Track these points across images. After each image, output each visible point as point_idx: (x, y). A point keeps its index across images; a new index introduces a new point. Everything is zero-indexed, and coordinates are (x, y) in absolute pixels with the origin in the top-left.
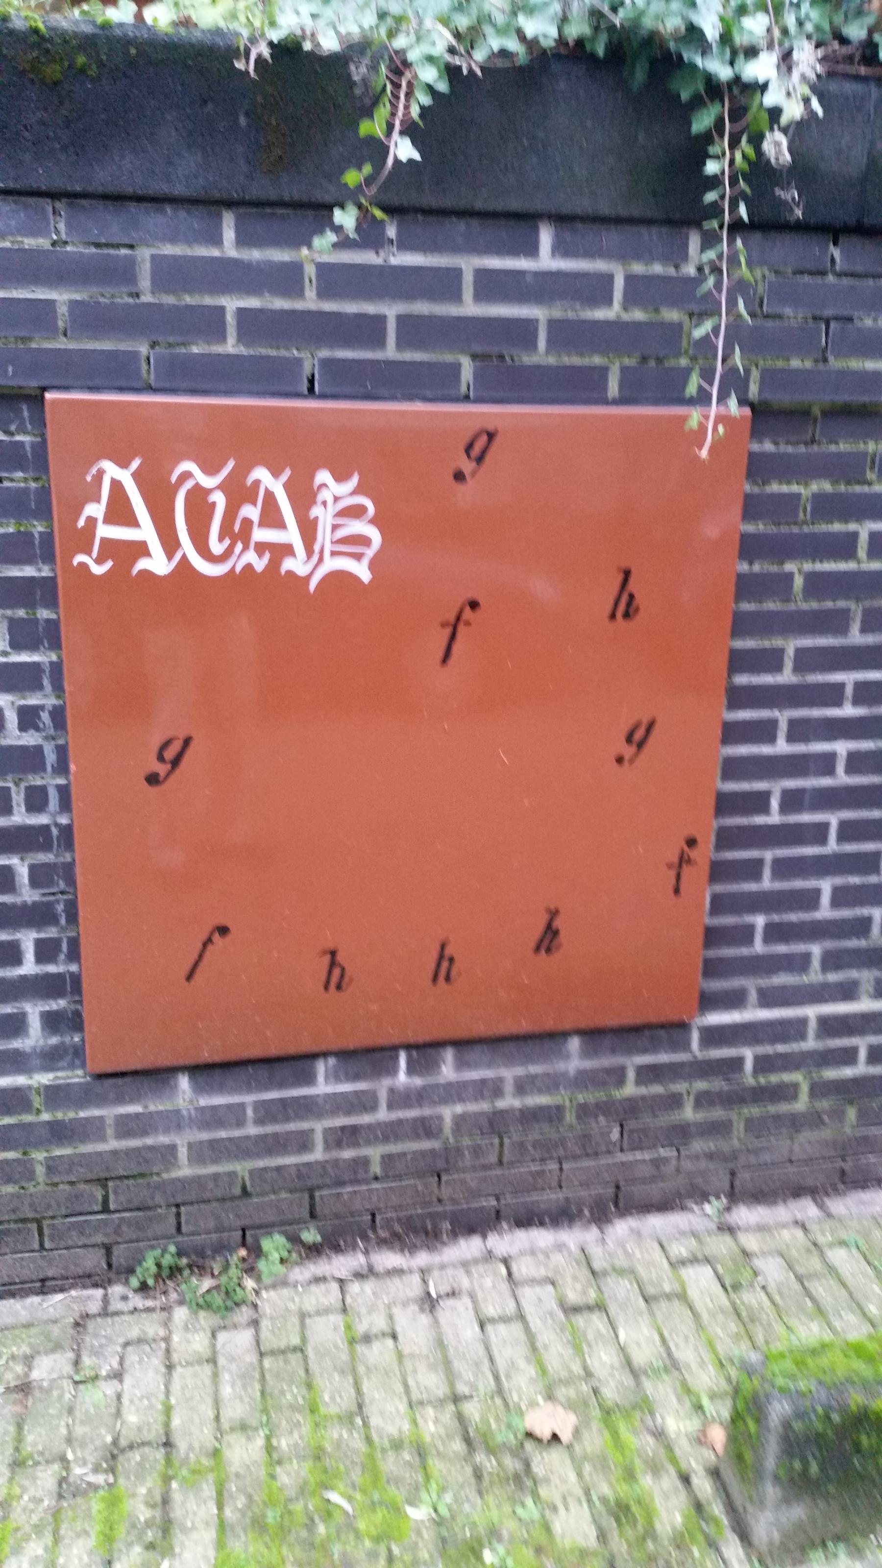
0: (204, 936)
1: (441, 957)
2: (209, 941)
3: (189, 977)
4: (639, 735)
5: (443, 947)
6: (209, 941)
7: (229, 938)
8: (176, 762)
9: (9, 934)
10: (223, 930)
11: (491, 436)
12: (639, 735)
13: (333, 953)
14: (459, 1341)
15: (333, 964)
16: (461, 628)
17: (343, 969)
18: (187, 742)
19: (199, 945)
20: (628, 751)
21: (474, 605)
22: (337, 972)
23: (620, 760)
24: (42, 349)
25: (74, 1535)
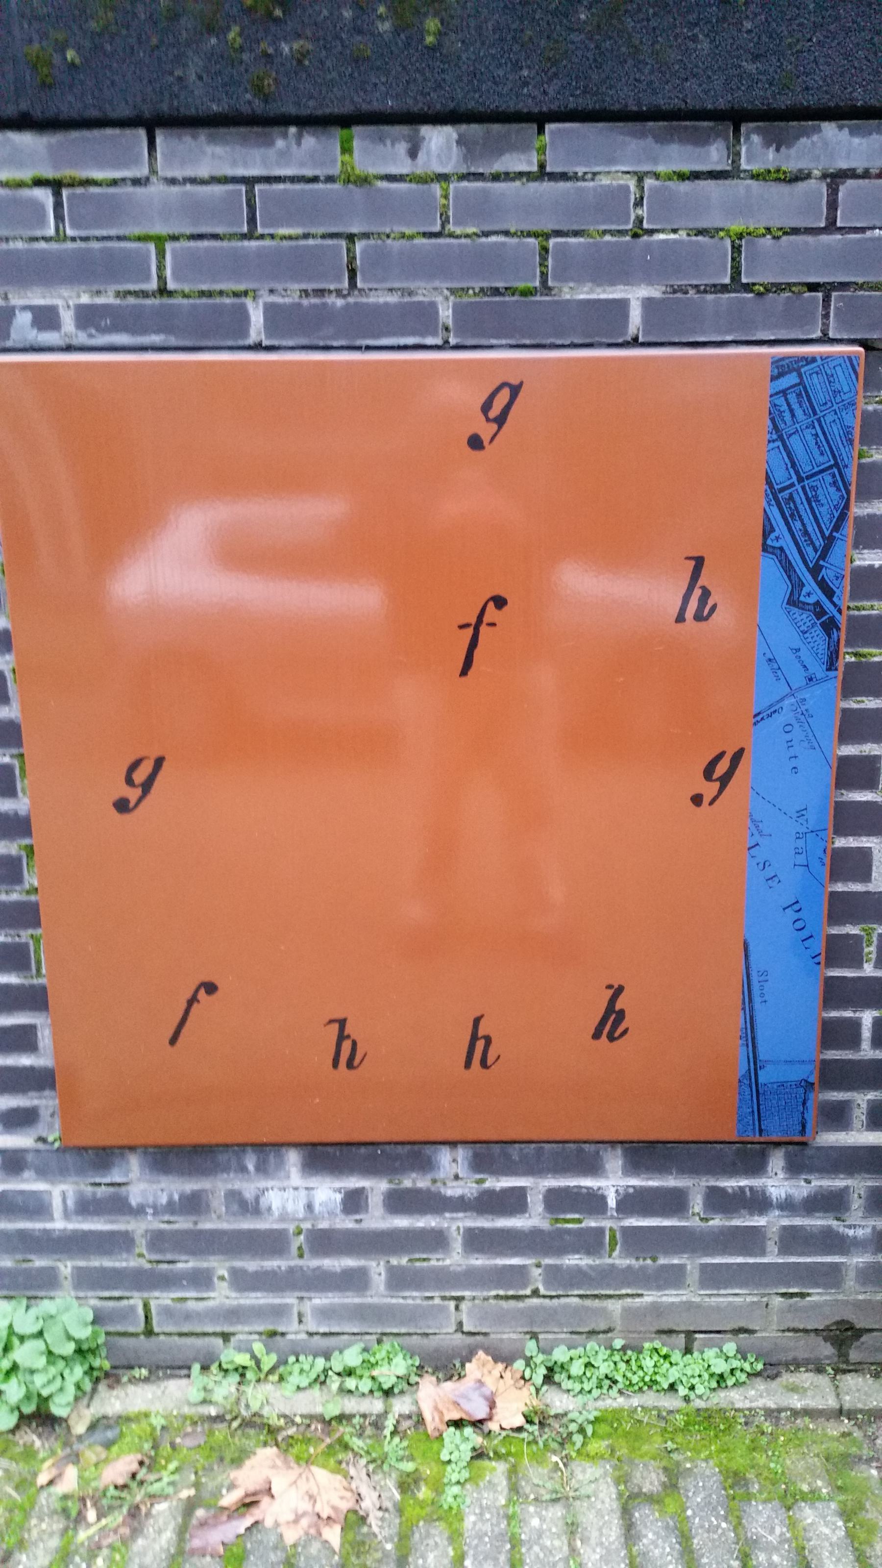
0: (189, 995)
1: (474, 1038)
2: (193, 1001)
3: (173, 1041)
4: (722, 768)
5: (477, 1021)
6: (193, 1001)
7: (214, 997)
8: (147, 786)
9: (106, 1222)
10: (211, 988)
11: (515, 390)
12: (722, 768)
13: (342, 1023)
14: (152, 1483)
15: (342, 1037)
16: (483, 629)
17: (354, 1044)
18: (159, 762)
19: (184, 1005)
20: (710, 789)
21: (500, 602)
22: (346, 1046)
23: (697, 800)
24: (201, 1232)
25: (302, 1455)
